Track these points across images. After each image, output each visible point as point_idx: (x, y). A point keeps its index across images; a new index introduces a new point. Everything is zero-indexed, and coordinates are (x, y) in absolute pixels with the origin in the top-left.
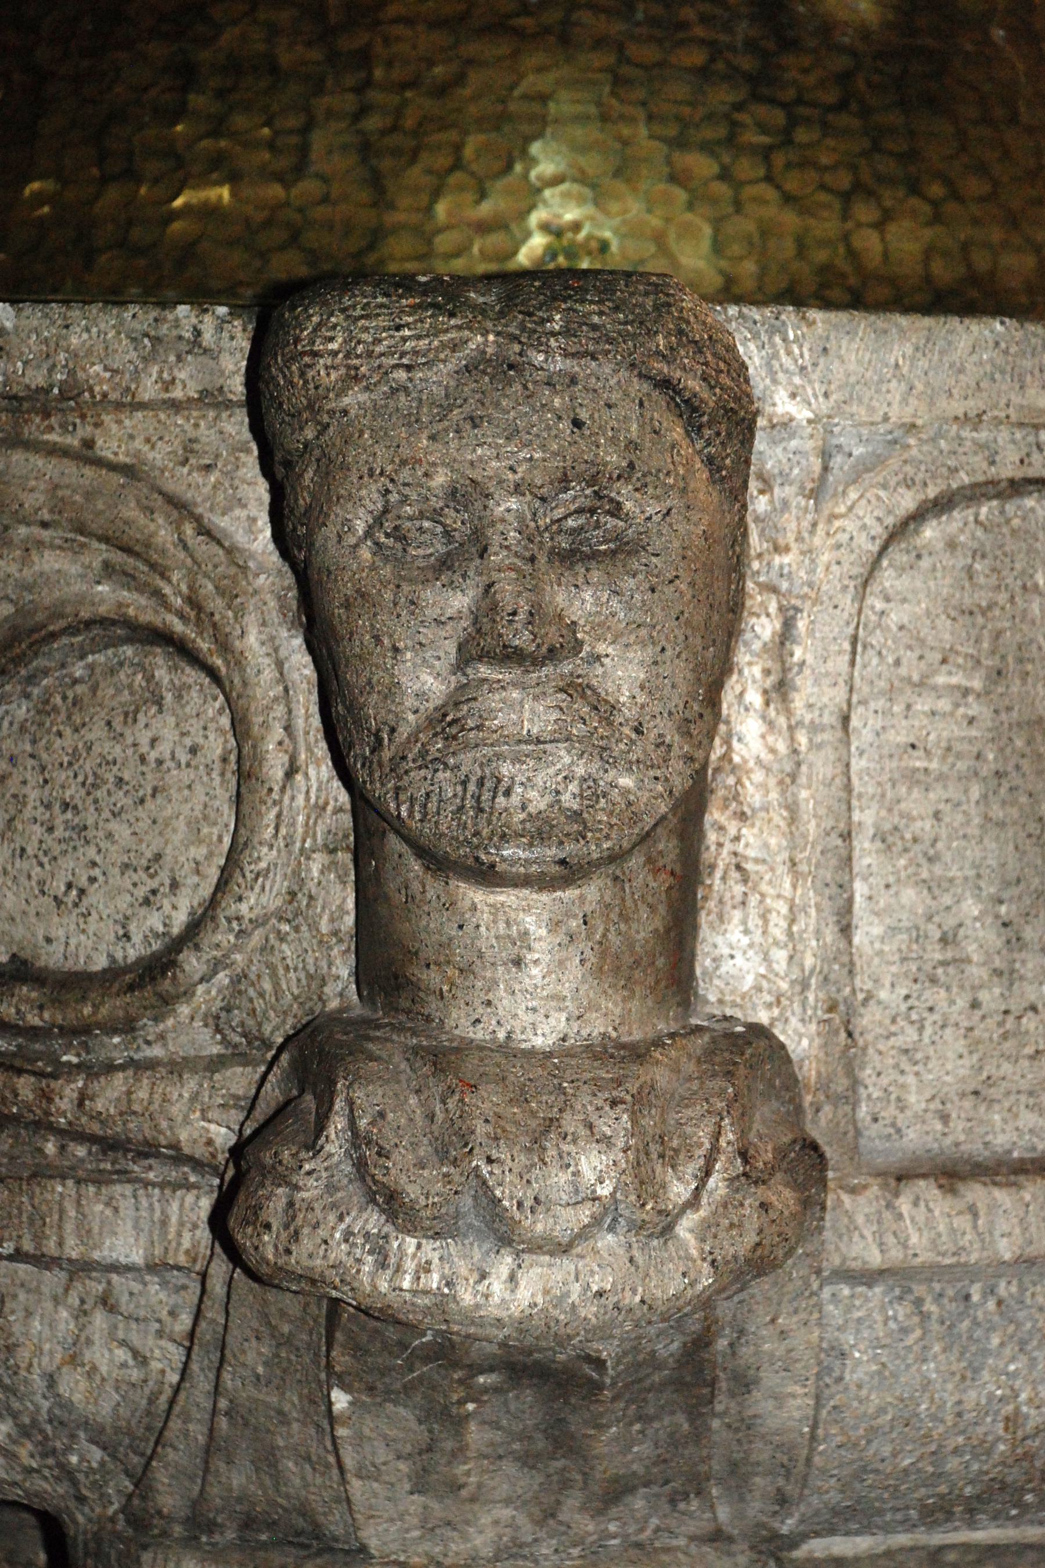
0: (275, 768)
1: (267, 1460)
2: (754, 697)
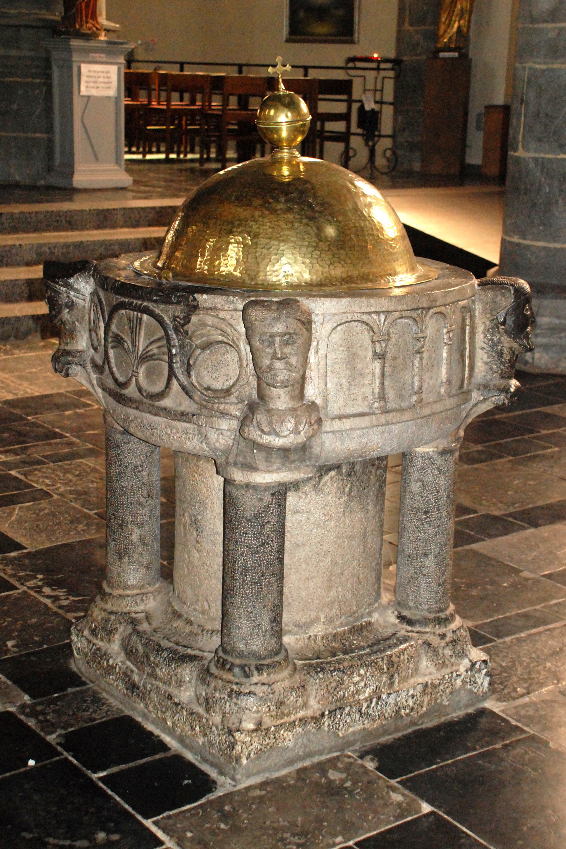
0: (245, 365)
1: (245, 457)
2: (313, 353)
